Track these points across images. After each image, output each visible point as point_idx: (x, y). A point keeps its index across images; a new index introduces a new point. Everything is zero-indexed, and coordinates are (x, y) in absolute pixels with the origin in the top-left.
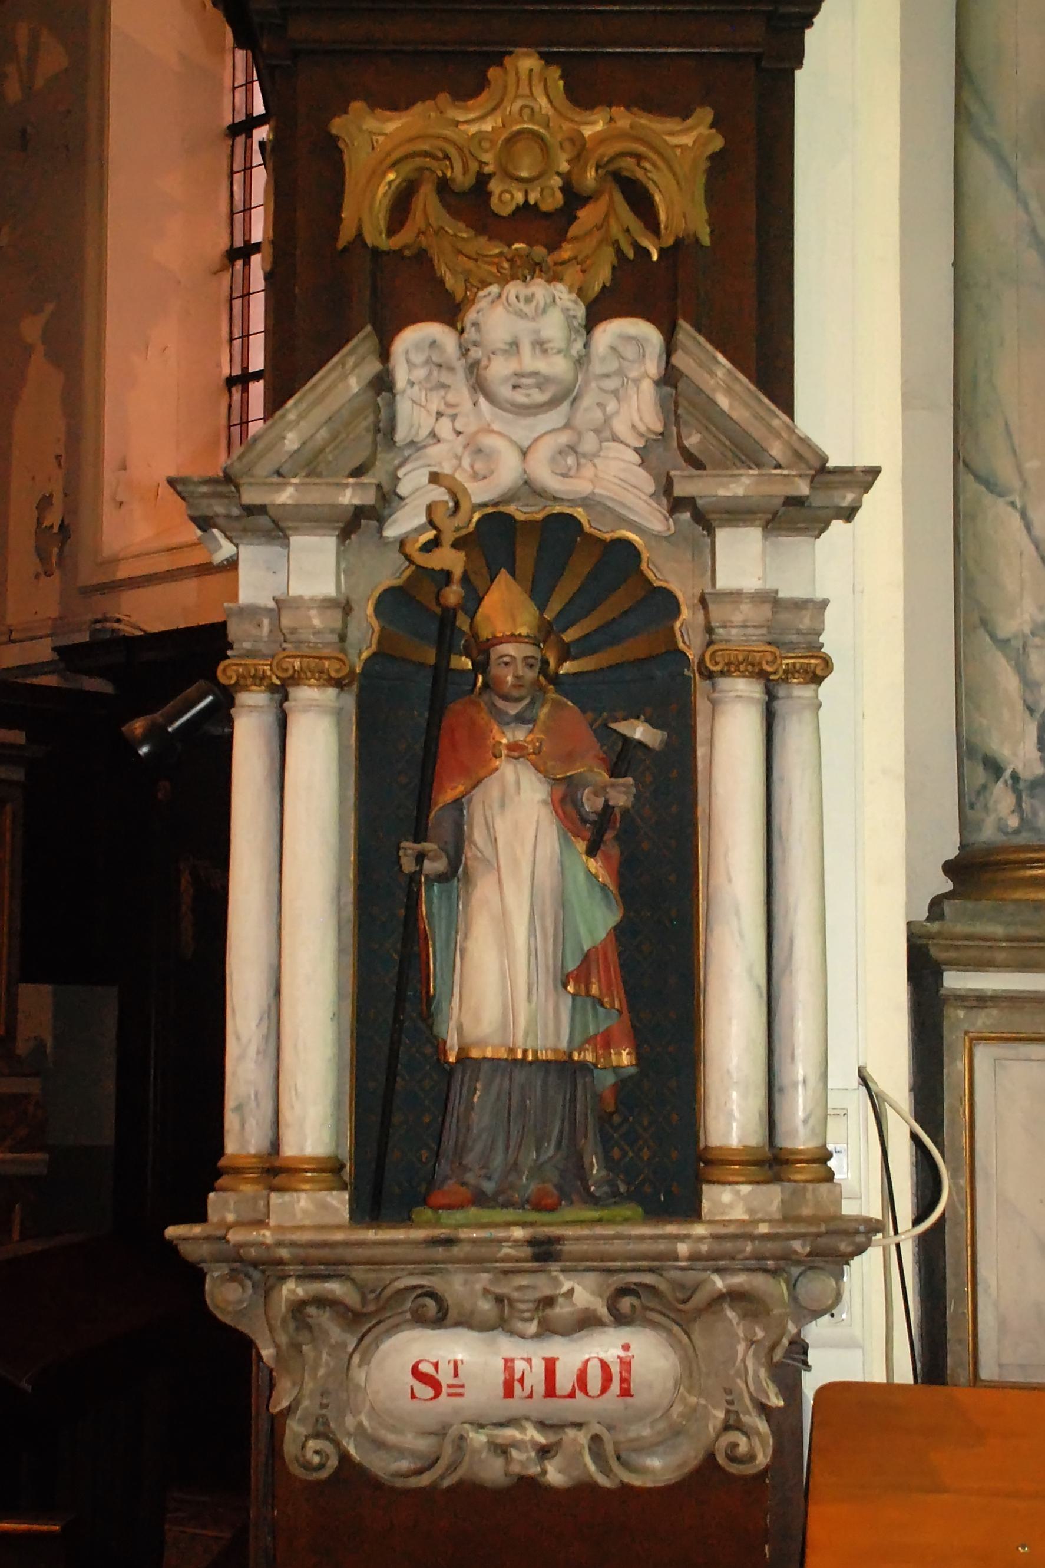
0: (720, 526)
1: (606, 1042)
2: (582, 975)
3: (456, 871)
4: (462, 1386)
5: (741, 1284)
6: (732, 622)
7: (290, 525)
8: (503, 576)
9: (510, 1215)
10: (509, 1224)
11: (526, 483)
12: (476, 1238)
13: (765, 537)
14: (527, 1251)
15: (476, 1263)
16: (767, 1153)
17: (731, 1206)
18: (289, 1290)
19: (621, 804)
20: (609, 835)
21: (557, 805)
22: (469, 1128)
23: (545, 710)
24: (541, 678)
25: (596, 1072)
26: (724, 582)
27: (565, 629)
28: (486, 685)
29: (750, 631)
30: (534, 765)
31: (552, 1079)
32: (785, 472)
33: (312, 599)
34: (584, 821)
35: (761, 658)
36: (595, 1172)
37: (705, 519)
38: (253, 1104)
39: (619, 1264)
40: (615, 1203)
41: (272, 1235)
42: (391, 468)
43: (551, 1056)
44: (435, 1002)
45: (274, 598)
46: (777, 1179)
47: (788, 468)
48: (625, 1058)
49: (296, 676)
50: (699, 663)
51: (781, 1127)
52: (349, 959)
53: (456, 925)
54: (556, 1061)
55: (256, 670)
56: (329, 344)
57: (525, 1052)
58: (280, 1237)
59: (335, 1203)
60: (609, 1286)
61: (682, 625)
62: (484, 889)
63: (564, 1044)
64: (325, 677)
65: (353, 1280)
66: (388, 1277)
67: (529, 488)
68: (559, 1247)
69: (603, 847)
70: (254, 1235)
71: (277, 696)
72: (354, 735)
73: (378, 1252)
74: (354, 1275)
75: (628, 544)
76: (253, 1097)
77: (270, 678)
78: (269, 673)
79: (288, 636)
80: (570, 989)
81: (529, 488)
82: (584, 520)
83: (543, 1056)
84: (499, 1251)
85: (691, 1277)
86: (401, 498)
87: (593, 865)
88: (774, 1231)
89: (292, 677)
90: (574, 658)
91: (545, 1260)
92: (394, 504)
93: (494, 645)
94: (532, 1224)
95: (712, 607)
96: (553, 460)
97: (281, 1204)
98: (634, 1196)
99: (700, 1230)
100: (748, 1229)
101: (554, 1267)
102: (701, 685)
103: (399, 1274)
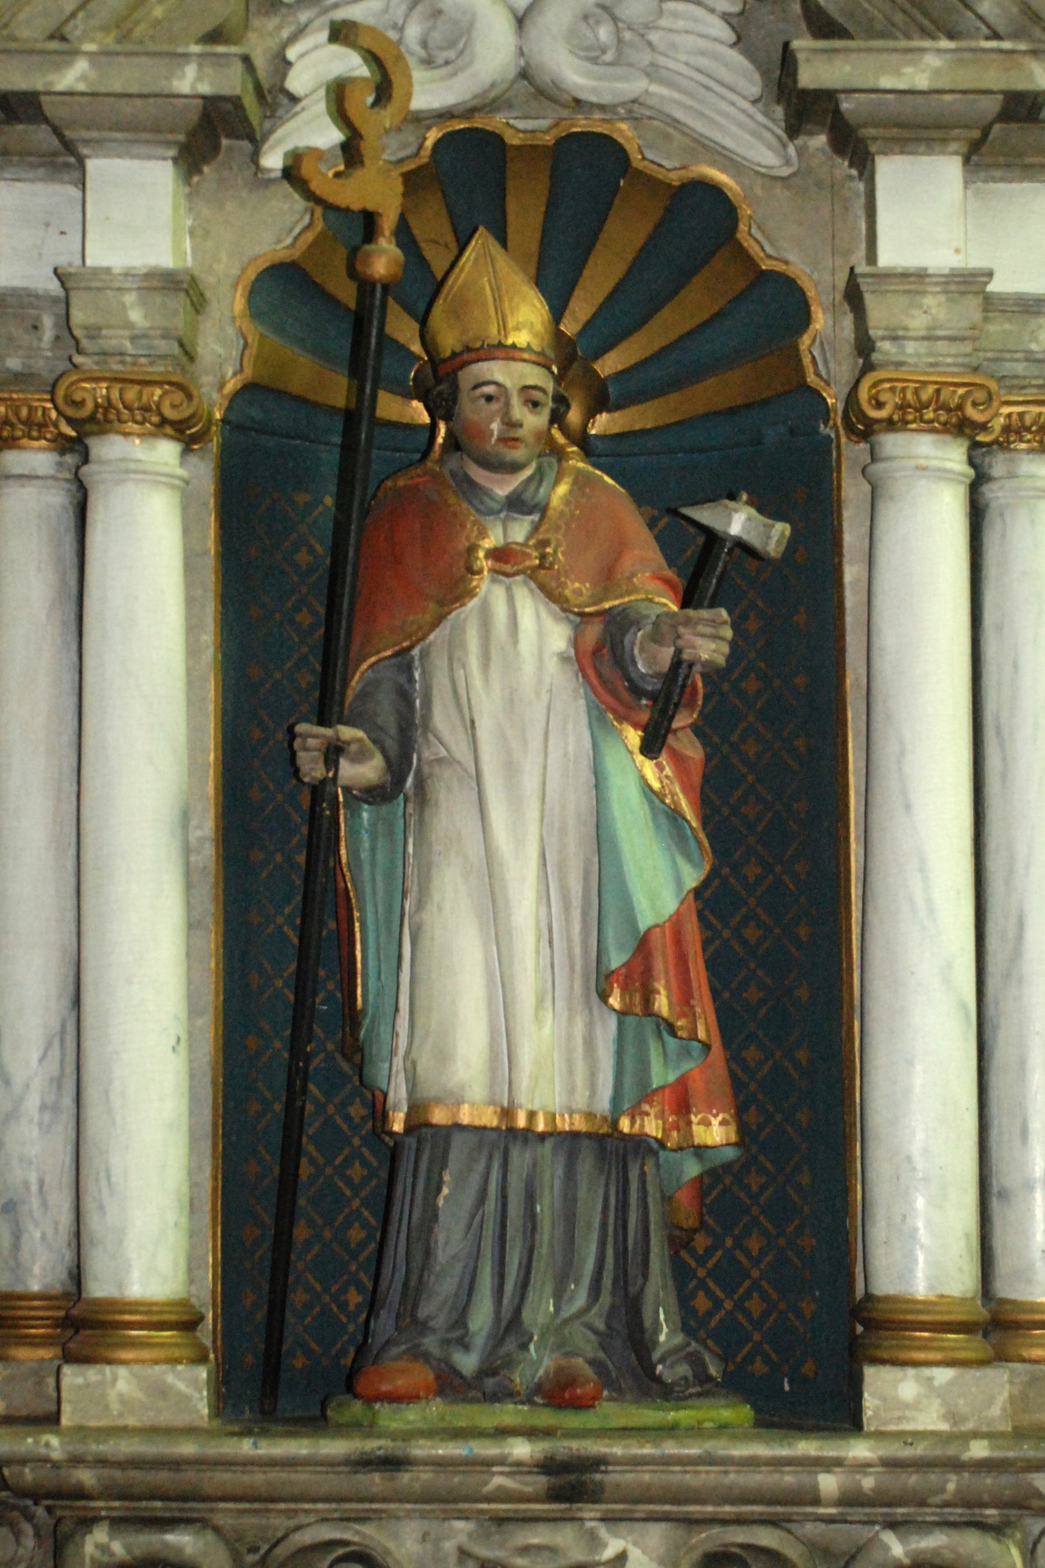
0: (885, 153)
1: (681, 1102)
2: (638, 977)
3: (403, 781)
5: (936, 1551)
6: (906, 329)
7: (85, 134)
8: (482, 241)
9: (508, 1414)
10: (502, 1433)
11: (524, 74)
12: (443, 1457)
13: (967, 183)
14: (541, 1482)
15: (443, 1502)
16: (981, 1313)
17: (915, 1406)
18: (97, 1546)
19: (705, 656)
20: (682, 720)
21: (587, 661)
22: (428, 1253)
23: (562, 489)
24: (556, 433)
25: (662, 1154)
27: (599, 353)
28: (454, 444)
29: (942, 346)
30: (542, 587)
31: (586, 1165)
32: (1007, 45)
33: (127, 274)
34: (637, 691)
35: (963, 397)
36: (662, 1338)
38: (35, 1202)
39: (710, 1509)
40: (699, 1395)
41: (62, 1444)
42: (273, 44)
43: (580, 1124)
44: (366, 1022)
45: (55, 271)
46: (1001, 1357)
47: (1014, 36)
48: (714, 1131)
49: (99, 416)
50: (846, 412)
51: (1003, 1264)
52: (210, 941)
53: (407, 888)
54: (589, 1135)
55: (31, 408)
57: (532, 1115)
58: (79, 1448)
59: (181, 1386)
60: (692, 1548)
61: (814, 341)
62: (451, 813)
63: (604, 1104)
64: (155, 419)
65: (217, 1530)
66: (279, 1523)
67: (531, 83)
68: (598, 1477)
69: (671, 739)
70: (29, 1443)
71: (70, 459)
72: (212, 532)
73: (258, 1478)
74: (220, 1520)
75: (715, 191)
76: (34, 1188)
78: (54, 414)
79: (85, 343)
80: (615, 1001)
81: (531, 83)
82: (631, 148)
83: (564, 1124)
84: (486, 1484)
85: (842, 1536)
86: (294, 99)
87: (649, 769)
88: (998, 1454)
89: (92, 419)
90: (618, 407)
91: (570, 1500)
92: (280, 112)
93: (465, 364)
94: (548, 1433)
95: (869, 300)
96: (572, 35)
97: (80, 1387)
98: (735, 1384)
99: (860, 1450)
100: (951, 1451)
101: (590, 1512)
102: (853, 452)
103: (303, 1519)
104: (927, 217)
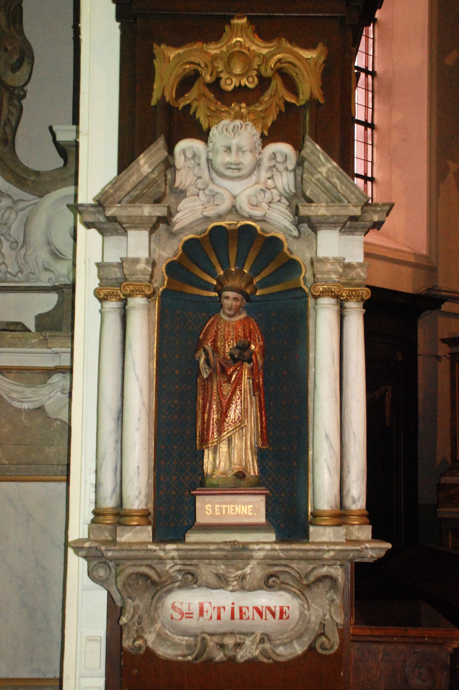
4: (192, 614)
26: (321, 254)
37: (314, 225)
56: (143, 146)
77: (119, 295)
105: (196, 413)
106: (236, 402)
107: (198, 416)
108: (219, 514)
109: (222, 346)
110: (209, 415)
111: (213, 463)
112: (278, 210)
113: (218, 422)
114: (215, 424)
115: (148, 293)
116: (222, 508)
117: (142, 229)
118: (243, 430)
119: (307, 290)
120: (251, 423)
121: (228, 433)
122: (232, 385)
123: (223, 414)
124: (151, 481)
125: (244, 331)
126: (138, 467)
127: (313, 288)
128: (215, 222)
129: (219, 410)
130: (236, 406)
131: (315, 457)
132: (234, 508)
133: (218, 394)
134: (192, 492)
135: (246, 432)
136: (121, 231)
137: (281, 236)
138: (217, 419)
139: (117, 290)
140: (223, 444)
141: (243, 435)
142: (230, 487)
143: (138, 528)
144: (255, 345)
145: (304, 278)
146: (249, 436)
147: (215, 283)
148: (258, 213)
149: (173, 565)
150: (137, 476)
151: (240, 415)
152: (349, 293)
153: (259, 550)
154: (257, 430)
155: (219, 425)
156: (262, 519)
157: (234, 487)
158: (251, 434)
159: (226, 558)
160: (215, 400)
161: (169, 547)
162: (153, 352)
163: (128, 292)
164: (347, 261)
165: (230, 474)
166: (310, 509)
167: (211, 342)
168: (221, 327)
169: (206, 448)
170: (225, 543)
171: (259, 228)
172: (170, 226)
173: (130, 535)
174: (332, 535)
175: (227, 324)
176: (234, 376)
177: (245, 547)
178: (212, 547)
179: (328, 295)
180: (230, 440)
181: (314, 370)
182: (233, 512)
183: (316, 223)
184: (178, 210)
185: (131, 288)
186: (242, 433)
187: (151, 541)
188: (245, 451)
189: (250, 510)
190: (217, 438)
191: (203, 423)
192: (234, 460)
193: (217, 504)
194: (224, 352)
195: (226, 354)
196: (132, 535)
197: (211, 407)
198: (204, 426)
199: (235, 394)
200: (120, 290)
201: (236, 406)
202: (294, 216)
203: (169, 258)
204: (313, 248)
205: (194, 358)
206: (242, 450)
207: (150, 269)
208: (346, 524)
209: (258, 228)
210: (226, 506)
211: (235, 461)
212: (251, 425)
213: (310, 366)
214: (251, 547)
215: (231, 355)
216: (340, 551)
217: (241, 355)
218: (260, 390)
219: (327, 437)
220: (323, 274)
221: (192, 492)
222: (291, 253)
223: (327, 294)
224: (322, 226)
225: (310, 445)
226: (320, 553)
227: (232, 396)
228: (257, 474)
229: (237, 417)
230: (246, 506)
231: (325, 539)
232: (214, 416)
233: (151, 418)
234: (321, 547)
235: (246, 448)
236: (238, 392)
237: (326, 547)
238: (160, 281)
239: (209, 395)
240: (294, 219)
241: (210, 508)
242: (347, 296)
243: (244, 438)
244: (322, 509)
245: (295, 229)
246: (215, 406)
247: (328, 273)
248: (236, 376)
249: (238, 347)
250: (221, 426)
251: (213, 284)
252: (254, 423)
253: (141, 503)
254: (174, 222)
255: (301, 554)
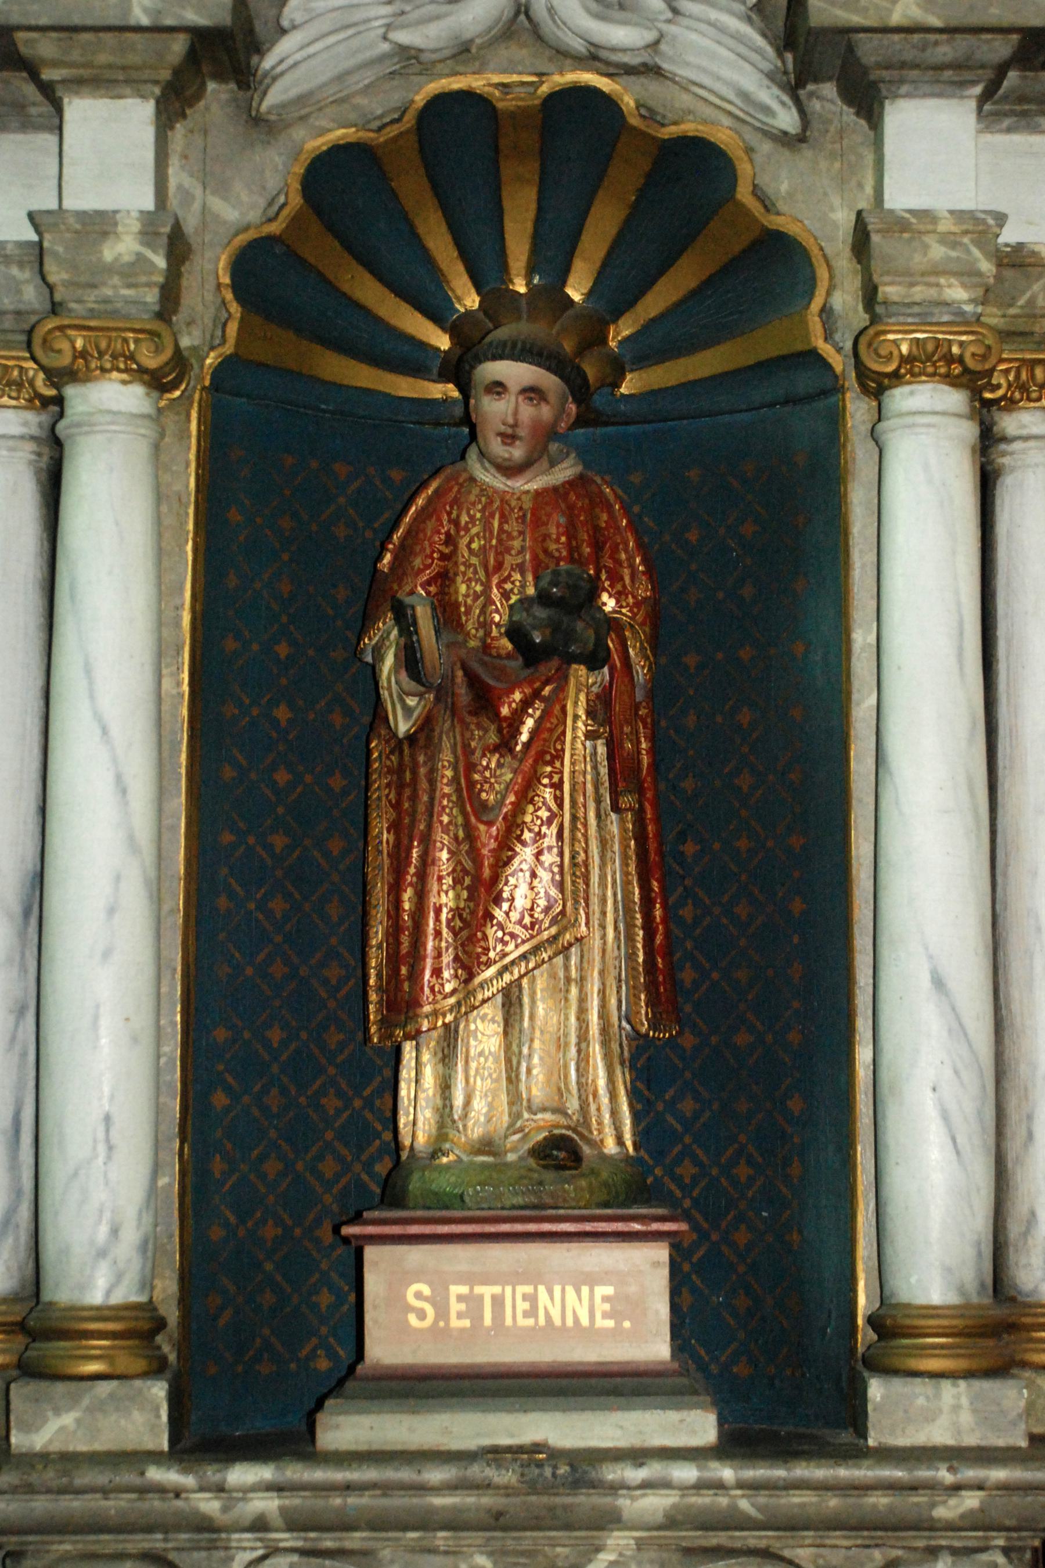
26: (901, 195)
77: (32, 383)
104: (935, 155)
105: (365, 891)
106: (540, 836)
107: (374, 902)
108: (466, 1323)
109: (477, 596)
110: (421, 895)
111: (439, 1102)
112: (710, 23)
113: (458, 923)
114: (445, 931)
115: (152, 362)
116: (481, 1297)
117: (128, 91)
118: (567, 959)
119: (838, 362)
120: (603, 927)
121: (505, 968)
122: (521, 761)
123: (483, 888)
124: (170, 1180)
125: (571, 531)
126: (108, 1119)
127: (870, 345)
128: (441, 76)
129: (466, 872)
130: (539, 854)
131: (884, 1075)
132: (532, 1299)
133: (460, 804)
134: (347, 1230)
135: (581, 968)
136: (40, 108)
137: (723, 135)
138: (457, 912)
139: (18, 358)
140: (483, 1018)
141: (568, 980)
142: (514, 1207)
143: (104, 1388)
144: (619, 596)
145: (826, 311)
146: (594, 987)
147: (443, 342)
148: (622, 36)
149: (260, 1552)
150: (101, 1160)
151: (554, 892)
152: (1018, 376)
153: (646, 1485)
154: (631, 957)
155: (465, 934)
156: (656, 1348)
157: (535, 1207)
158: (602, 973)
159: (497, 1521)
160: (446, 830)
161: (242, 1474)
162: (178, 624)
163: (65, 360)
164: (1009, 236)
165: (513, 1150)
166: (862, 1300)
167: (429, 583)
168: (472, 518)
169: (408, 1037)
170: (495, 1454)
171: (632, 104)
172: (249, 93)
173: (68, 1419)
174: (966, 1418)
175: (497, 504)
176: (530, 723)
177: (582, 1466)
178: (435, 1475)
179: (934, 374)
180: (511, 1001)
181: (873, 700)
182: (526, 1314)
183: (879, 66)
184: (285, 23)
185: (79, 343)
186: (567, 968)
187: (165, 1446)
188: (579, 1051)
189: (601, 1307)
190: (454, 992)
191: (395, 930)
192: (529, 1089)
193: (459, 1281)
194: (485, 625)
195: (495, 632)
196: (78, 1421)
197: (427, 861)
198: (399, 943)
199: (531, 801)
200: (33, 359)
201: (539, 854)
202: (780, 55)
203: (246, 228)
204: (860, 186)
205: (356, 653)
206: (567, 1044)
207: (161, 262)
208: (1024, 1365)
209: (628, 102)
210: (497, 1289)
211: (535, 1092)
212: (604, 937)
213: (856, 684)
214: (612, 1473)
215: (515, 632)
216: (1006, 1487)
217: (556, 636)
218: (641, 791)
219: (939, 983)
220: (912, 285)
221: (347, 1230)
222: (768, 206)
223: (930, 370)
224: (902, 81)
225: (863, 1025)
226: (919, 1499)
227: (518, 809)
228: (631, 1149)
229: (542, 903)
230: (585, 1290)
231: (939, 1435)
232: (444, 899)
233: (166, 908)
234: (924, 1473)
235: (583, 1037)
236: (548, 794)
237: (945, 1475)
238: (208, 321)
239: (421, 808)
240: (779, 64)
241: (412, 1309)
242: (1010, 385)
243: (574, 991)
244: (920, 1299)
245: (783, 104)
246: (444, 855)
247: (932, 279)
248: (539, 722)
249: (543, 598)
250: (471, 939)
251: (438, 349)
252: (616, 928)
253: (119, 1277)
254: (266, 74)
255: (833, 1502)
